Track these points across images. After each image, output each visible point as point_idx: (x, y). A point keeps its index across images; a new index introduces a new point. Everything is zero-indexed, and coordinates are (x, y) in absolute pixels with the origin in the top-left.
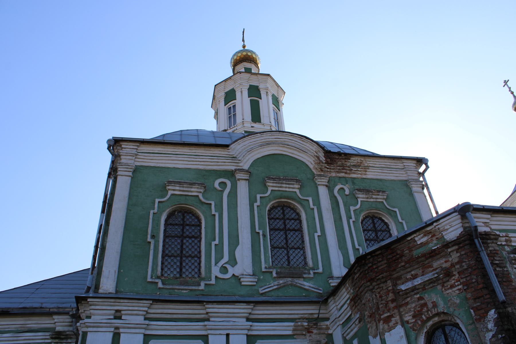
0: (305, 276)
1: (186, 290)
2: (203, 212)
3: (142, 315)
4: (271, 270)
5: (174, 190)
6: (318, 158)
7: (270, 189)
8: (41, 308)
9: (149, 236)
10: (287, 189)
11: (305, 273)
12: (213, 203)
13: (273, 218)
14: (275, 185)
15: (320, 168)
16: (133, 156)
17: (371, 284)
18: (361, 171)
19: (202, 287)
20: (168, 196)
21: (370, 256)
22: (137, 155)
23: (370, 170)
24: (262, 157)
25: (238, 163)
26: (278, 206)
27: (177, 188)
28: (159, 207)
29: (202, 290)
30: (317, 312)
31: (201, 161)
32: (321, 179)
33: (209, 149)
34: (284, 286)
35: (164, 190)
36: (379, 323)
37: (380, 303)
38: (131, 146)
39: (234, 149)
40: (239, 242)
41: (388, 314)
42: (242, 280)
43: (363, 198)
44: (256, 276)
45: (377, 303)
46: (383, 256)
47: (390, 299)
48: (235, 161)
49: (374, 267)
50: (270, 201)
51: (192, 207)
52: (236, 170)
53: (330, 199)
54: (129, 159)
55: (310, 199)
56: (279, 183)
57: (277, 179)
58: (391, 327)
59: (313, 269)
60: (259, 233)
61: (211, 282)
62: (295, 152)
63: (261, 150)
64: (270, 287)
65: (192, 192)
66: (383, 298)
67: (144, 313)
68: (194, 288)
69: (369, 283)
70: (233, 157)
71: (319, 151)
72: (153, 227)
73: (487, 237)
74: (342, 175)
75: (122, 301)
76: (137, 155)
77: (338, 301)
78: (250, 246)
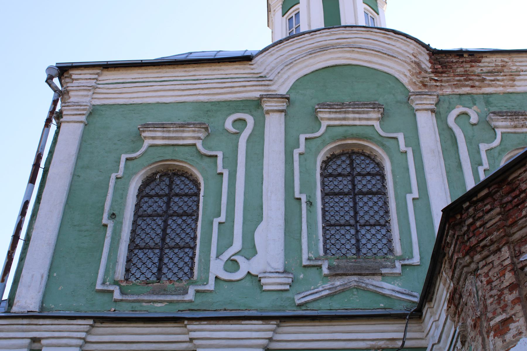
0: (384, 271)
2: (203, 171)
3: (76, 346)
4: (319, 263)
5: (154, 138)
6: (418, 64)
7: (324, 124)
9: (106, 216)
10: (357, 123)
11: (385, 267)
12: (220, 155)
13: (331, 175)
14: (333, 116)
15: (422, 82)
16: (89, 90)
17: (472, 258)
19: (190, 296)
20: (143, 149)
21: (468, 204)
23: (521, 77)
24: (313, 72)
25: (268, 85)
26: (343, 154)
27: (159, 134)
28: (126, 167)
29: (191, 302)
30: (401, 335)
31: (203, 89)
32: (421, 99)
33: (217, 67)
34: (343, 291)
35: (139, 139)
36: (488, 337)
37: (487, 296)
38: (87, 74)
39: (262, 63)
40: (262, 217)
41: (504, 316)
42: (263, 281)
43: (507, 127)
44: (289, 273)
45: (484, 296)
46: (495, 200)
47: (506, 284)
48: (263, 83)
49: (478, 224)
50: (324, 144)
51: (184, 165)
52: (262, 97)
53: (440, 134)
54: (82, 96)
55: (401, 137)
56: (340, 112)
57: (339, 106)
58: (509, 344)
59: (401, 258)
60: (299, 199)
61: (207, 288)
62: (375, 59)
63: (312, 61)
64: (316, 293)
65: (183, 138)
66: (494, 284)
67: (80, 342)
68: (175, 298)
69: (467, 258)
71: (420, 53)
72: (113, 201)
74: (467, 90)
75: (41, 321)
77: (437, 311)
78: (282, 222)
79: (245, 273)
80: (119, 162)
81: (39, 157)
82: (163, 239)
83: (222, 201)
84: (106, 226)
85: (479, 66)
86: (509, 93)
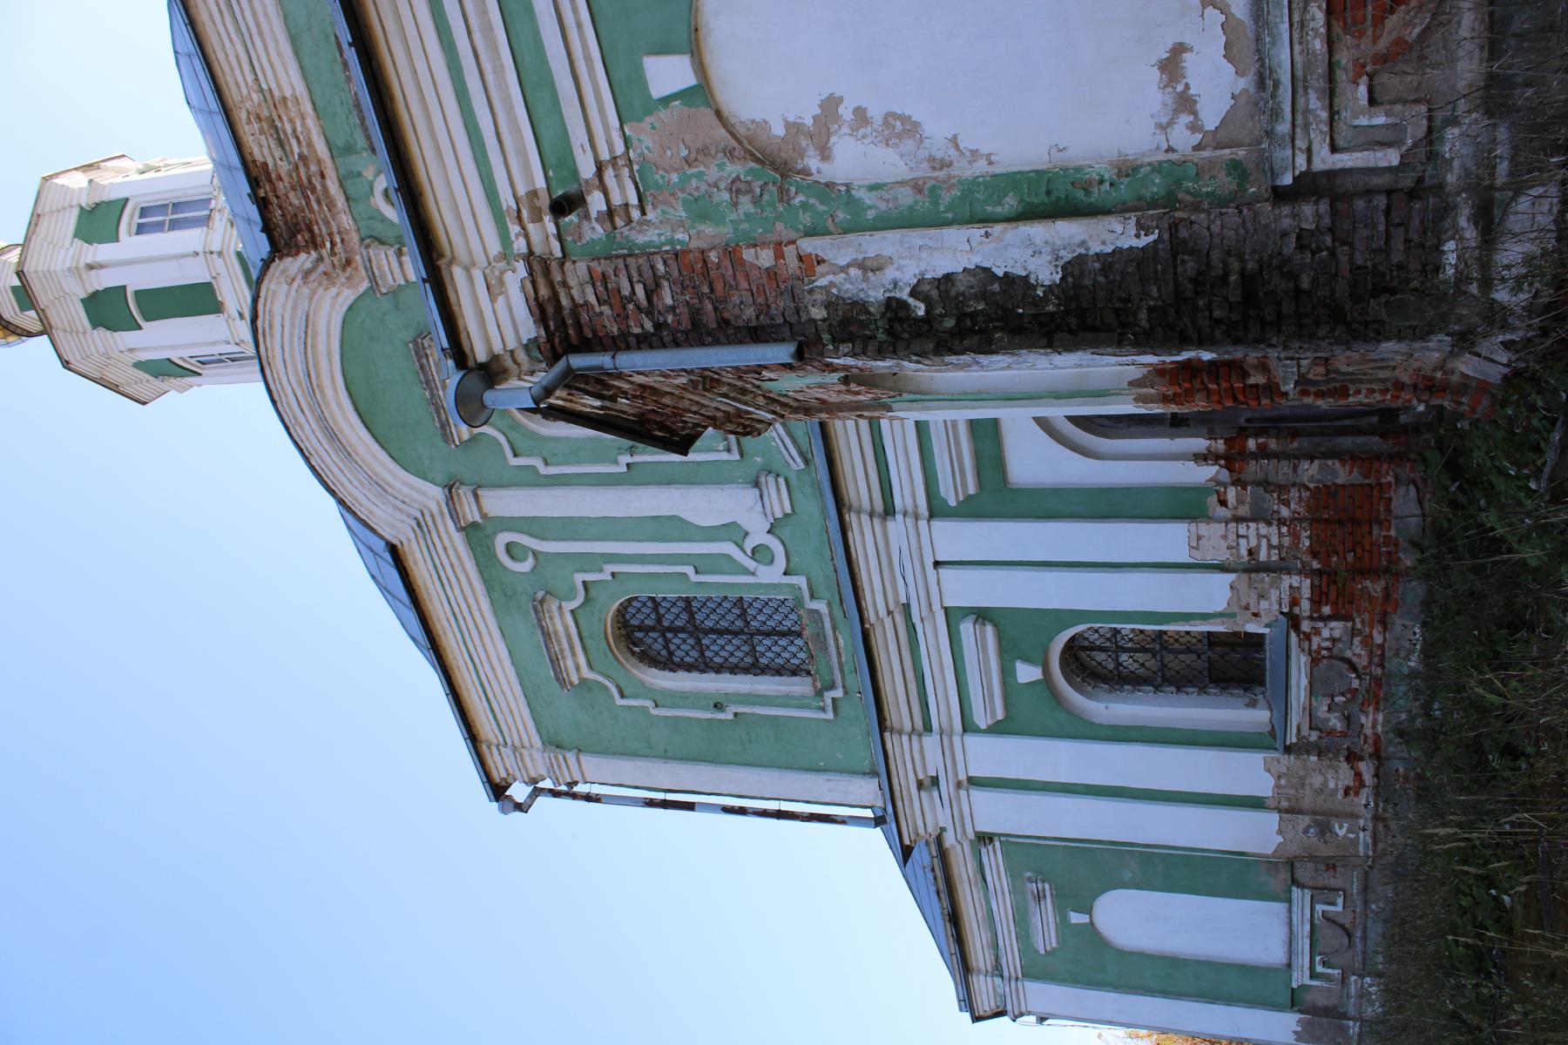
1: (836, 640)
5: (576, 665)
6: (307, 274)
8: (933, 870)
9: (721, 716)
12: (580, 578)
15: (344, 268)
18: (291, 121)
19: (821, 606)
20: (601, 679)
22: (515, 748)
23: (273, 86)
25: (432, 516)
27: (570, 663)
28: (635, 697)
29: (829, 604)
32: (383, 276)
39: (393, 527)
42: (779, 515)
52: (460, 529)
61: (804, 586)
62: (322, 347)
63: (362, 451)
65: (566, 628)
68: (828, 625)
70: (419, 525)
71: (283, 272)
72: (694, 707)
73: (550, 310)
74: (333, 187)
76: (515, 748)
79: (770, 537)
80: (630, 707)
81: (651, 803)
82: (736, 634)
83: (659, 568)
84: (736, 714)
85: (275, 164)
86: (315, 109)
